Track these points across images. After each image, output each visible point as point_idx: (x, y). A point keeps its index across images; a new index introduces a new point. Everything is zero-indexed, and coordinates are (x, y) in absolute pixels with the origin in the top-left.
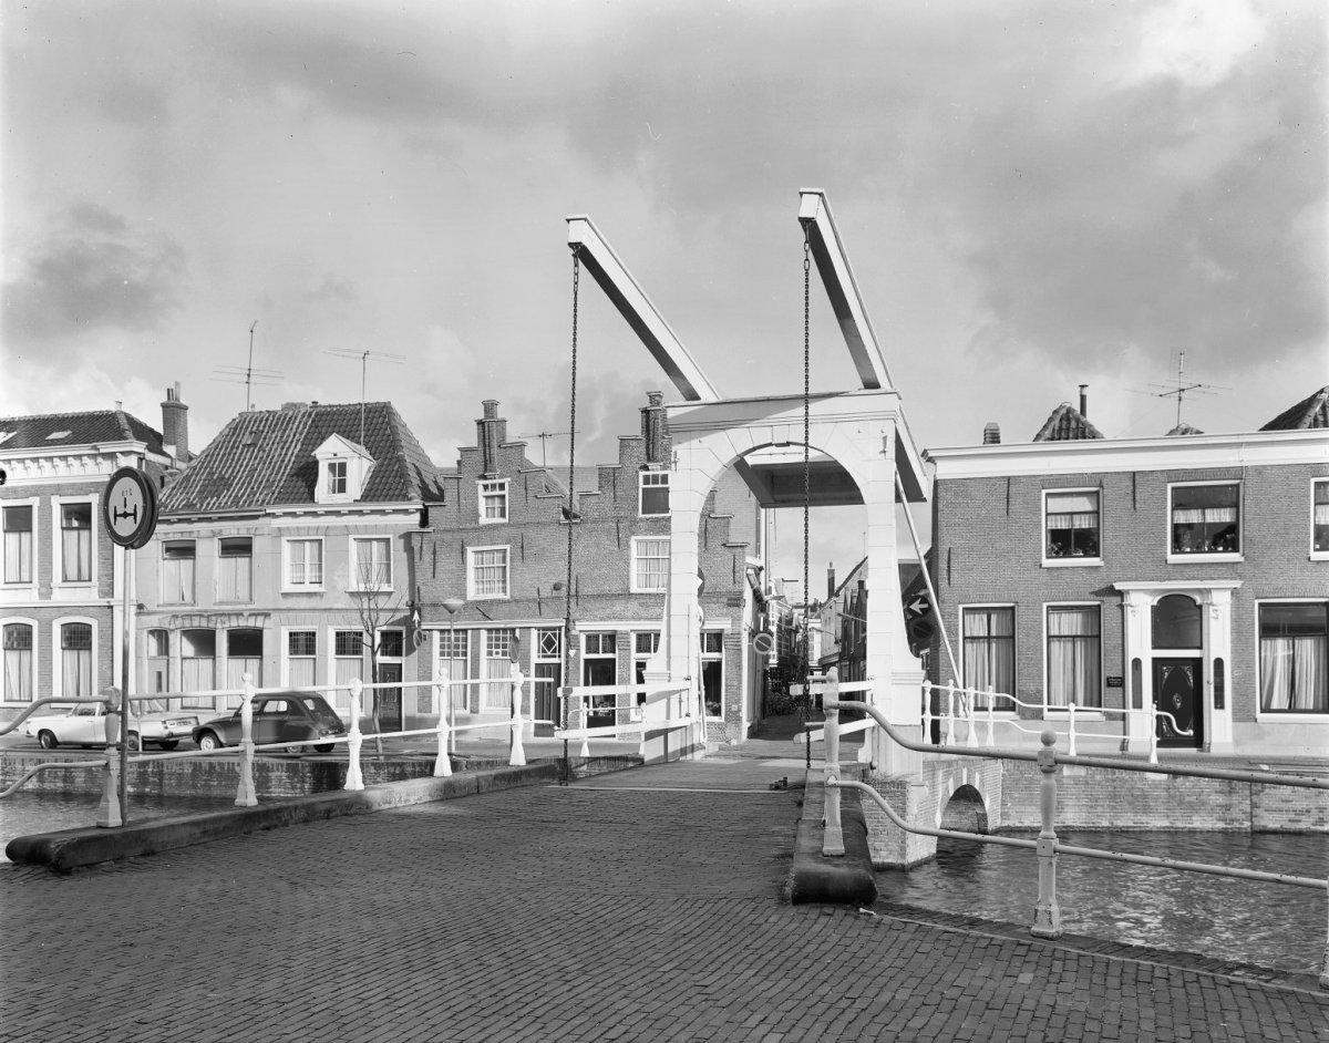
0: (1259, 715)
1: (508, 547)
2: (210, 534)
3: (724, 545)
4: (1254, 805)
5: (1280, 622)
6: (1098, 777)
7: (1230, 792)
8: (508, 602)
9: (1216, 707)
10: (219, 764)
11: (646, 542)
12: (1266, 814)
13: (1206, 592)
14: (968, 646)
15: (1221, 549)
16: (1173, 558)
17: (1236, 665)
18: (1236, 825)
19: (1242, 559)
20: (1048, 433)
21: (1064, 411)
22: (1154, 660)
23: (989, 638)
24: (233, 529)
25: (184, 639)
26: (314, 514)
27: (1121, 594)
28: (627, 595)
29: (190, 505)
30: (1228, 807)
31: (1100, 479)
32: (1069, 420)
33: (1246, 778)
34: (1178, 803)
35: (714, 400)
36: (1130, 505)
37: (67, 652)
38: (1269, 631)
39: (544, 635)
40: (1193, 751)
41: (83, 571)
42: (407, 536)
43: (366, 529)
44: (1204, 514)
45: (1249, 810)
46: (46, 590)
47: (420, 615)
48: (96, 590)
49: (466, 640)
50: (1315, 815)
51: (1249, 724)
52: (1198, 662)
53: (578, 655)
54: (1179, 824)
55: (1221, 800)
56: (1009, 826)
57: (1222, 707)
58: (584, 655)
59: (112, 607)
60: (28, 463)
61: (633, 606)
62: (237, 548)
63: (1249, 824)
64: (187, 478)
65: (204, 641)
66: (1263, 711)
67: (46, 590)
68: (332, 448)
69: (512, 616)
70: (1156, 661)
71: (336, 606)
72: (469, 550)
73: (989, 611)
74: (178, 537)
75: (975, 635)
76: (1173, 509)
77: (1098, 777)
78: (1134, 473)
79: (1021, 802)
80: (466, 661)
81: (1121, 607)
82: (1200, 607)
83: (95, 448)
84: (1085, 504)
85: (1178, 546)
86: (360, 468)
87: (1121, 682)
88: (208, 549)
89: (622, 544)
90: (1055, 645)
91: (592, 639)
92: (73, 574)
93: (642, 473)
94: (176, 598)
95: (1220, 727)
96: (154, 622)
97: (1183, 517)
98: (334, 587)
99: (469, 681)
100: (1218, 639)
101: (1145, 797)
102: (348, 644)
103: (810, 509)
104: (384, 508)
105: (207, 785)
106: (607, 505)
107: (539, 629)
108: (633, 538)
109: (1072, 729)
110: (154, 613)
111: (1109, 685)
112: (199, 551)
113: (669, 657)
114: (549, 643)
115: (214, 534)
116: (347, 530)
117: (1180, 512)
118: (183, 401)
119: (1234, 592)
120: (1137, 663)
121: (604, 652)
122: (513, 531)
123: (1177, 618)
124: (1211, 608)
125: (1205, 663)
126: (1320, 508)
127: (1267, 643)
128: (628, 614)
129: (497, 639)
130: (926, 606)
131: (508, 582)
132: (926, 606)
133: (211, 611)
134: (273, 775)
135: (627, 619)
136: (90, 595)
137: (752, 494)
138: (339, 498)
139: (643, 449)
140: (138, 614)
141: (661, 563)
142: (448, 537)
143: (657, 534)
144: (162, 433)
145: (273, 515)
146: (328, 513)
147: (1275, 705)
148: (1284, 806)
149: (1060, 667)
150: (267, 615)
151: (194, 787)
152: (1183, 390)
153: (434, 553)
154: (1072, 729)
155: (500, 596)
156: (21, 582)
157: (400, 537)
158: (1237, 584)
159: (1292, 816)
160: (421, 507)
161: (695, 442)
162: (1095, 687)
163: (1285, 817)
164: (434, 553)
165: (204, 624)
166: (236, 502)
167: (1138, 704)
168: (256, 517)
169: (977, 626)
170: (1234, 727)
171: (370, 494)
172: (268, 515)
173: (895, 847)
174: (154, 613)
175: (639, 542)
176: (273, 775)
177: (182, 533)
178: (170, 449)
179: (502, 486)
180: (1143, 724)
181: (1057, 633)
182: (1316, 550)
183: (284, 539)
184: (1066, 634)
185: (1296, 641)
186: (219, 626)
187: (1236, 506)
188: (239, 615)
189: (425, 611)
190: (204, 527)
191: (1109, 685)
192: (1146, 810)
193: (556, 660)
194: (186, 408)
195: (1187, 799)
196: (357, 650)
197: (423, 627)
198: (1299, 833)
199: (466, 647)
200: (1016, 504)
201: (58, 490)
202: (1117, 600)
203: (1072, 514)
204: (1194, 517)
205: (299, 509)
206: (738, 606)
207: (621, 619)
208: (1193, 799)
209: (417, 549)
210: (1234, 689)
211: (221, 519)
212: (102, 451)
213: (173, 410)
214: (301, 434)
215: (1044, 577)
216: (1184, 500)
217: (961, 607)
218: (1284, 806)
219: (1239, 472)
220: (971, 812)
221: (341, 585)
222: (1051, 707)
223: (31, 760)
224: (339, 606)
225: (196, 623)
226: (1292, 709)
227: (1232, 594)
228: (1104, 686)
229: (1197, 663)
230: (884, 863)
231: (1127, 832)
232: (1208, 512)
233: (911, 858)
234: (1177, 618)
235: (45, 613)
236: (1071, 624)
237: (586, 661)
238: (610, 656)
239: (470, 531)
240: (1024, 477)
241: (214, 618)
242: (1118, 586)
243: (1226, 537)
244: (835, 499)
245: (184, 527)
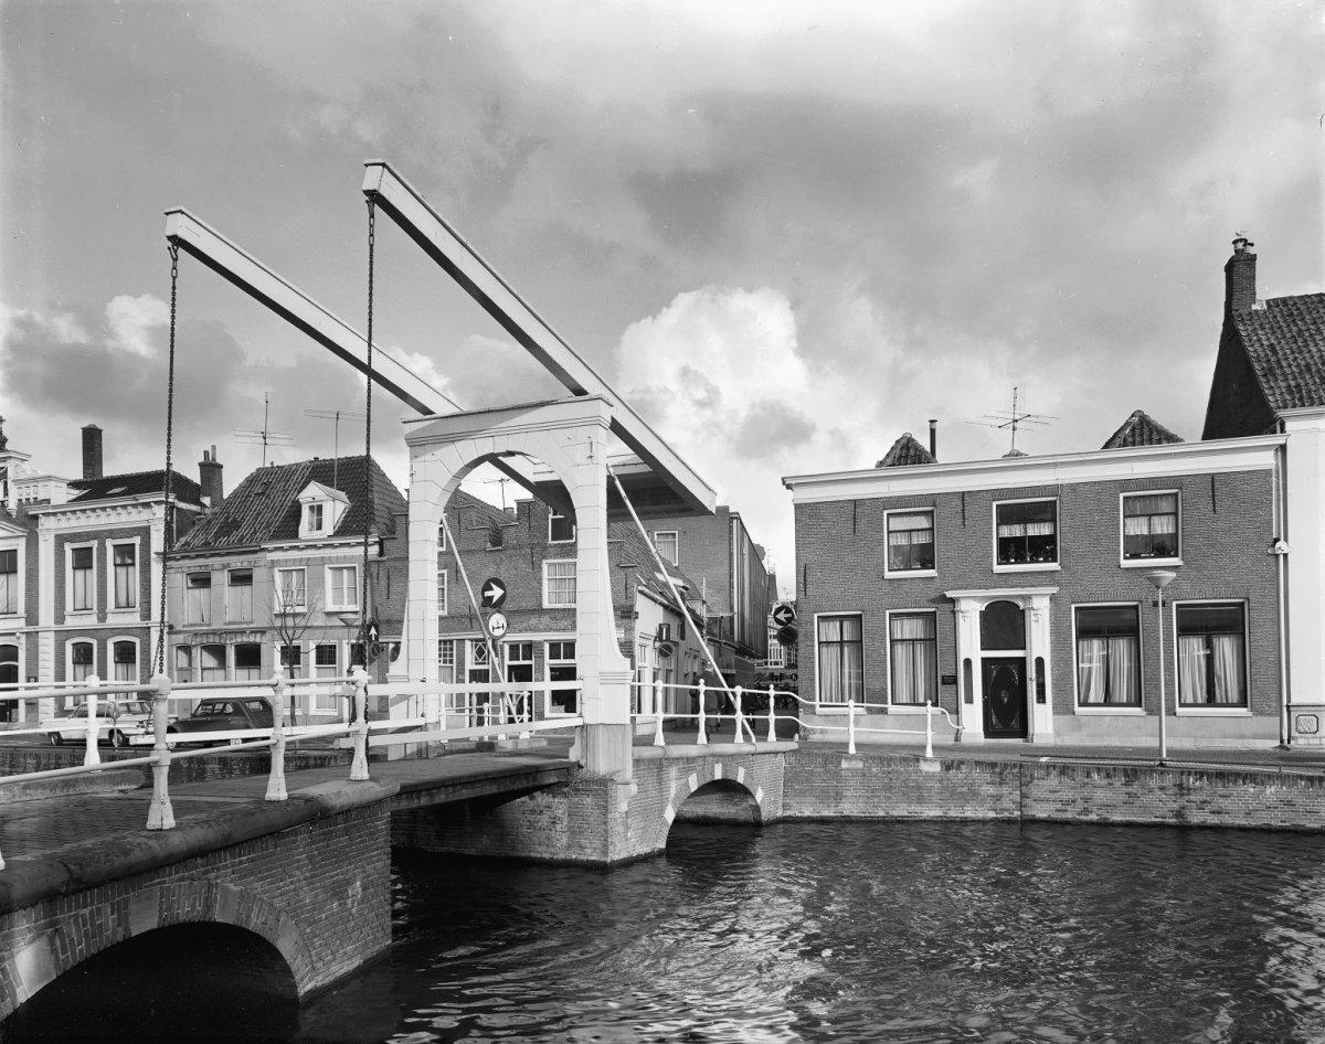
0: (1077, 709)
3: (618, 565)
4: (1024, 796)
5: (1098, 624)
6: (874, 770)
7: (1001, 784)
9: (1038, 702)
11: (555, 564)
12: (1034, 804)
13: (1027, 598)
14: (824, 650)
15: (1041, 559)
16: (998, 569)
17: (1055, 664)
18: (1006, 814)
19: (1059, 568)
20: (889, 461)
21: (904, 441)
22: (983, 659)
23: (841, 643)
24: (238, 562)
25: (205, 653)
26: (297, 548)
27: (953, 601)
28: (540, 611)
29: (207, 544)
30: (998, 798)
31: (933, 499)
32: (908, 449)
33: (1066, 763)
34: (952, 794)
35: (452, 410)
36: (960, 522)
37: (119, 665)
38: (1085, 633)
39: (476, 645)
40: (1019, 741)
41: (120, 597)
44: (1025, 529)
45: (1019, 800)
46: (102, 617)
47: (377, 630)
49: (451, 649)
50: (1080, 805)
51: (1068, 717)
52: (1023, 660)
54: (952, 814)
55: (991, 790)
56: (790, 816)
57: (1044, 702)
58: (508, 662)
59: (149, 628)
60: (69, 515)
61: (546, 619)
62: (241, 578)
63: (1019, 813)
64: (209, 522)
65: (218, 652)
66: (1080, 705)
67: (102, 617)
68: (314, 491)
70: (985, 661)
71: (315, 624)
73: (842, 618)
74: (197, 570)
75: (905, 637)
76: (998, 525)
77: (874, 770)
78: (963, 493)
79: (802, 793)
81: (954, 612)
82: (1023, 611)
83: (135, 499)
84: (923, 523)
85: (1004, 558)
86: (335, 508)
87: (953, 680)
88: (221, 579)
89: (537, 568)
90: (899, 648)
91: (514, 648)
92: (123, 601)
94: (199, 621)
95: (1043, 721)
96: (180, 639)
97: (1006, 532)
99: (637, 684)
100: (1039, 641)
101: (919, 788)
103: (164, 468)
104: (348, 541)
106: (524, 534)
107: (471, 640)
108: (544, 561)
109: (852, 725)
110: (181, 632)
111: (944, 683)
112: (213, 581)
114: (480, 652)
115: (224, 567)
117: (1005, 527)
118: (219, 461)
119: (1053, 598)
120: (968, 663)
123: (1004, 623)
124: (1032, 612)
125: (1028, 661)
126: (1128, 521)
127: (1084, 644)
128: (541, 627)
129: (445, 649)
130: (789, 615)
131: (446, 602)
132: (789, 615)
134: (208, 767)
135: (540, 631)
136: (133, 619)
137: (405, 495)
138: (317, 534)
140: (169, 633)
141: (569, 583)
144: (199, 483)
147: (1091, 700)
148: (1052, 796)
149: (906, 670)
150: (262, 632)
152: (1017, 421)
153: (388, 578)
154: (852, 725)
156: (86, 609)
158: (1055, 590)
159: (1059, 806)
160: (377, 539)
161: (428, 457)
162: (934, 686)
163: (1052, 806)
164: (388, 578)
166: (241, 540)
167: (969, 700)
168: (255, 552)
169: (832, 632)
170: (1055, 721)
171: (343, 530)
172: (263, 550)
173: (597, 844)
174: (181, 632)
175: (549, 565)
176: (208, 767)
178: (206, 501)
180: (972, 717)
181: (899, 637)
182: (1125, 558)
184: (908, 637)
185: (1110, 642)
187: (1054, 520)
188: (242, 632)
189: (382, 628)
190: (216, 561)
191: (944, 683)
192: (920, 800)
194: (221, 467)
195: (959, 790)
197: (380, 640)
198: (1065, 823)
199: (451, 655)
200: (862, 523)
201: (112, 534)
202: (948, 606)
203: (910, 531)
204: (1016, 531)
205: (285, 545)
206: (629, 617)
207: (536, 631)
208: (965, 789)
210: (1054, 685)
211: (228, 554)
212: (141, 501)
213: (211, 469)
215: (887, 588)
216: (1008, 515)
217: (816, 616)
218: (1052, 796)
219: (1055, 489)
220: (744, 804)
221: (319, 606)
222: (823, 703)
225: (212, 640)
226: (1108, 702)
227: (1051, 600)
229: (1021, 663)
230: (588, 861)
231: (908, 821)
232: (1029, 526)
233: (618, 852)
234: (1004, 623)
235: (102, 634)
236: (912, 629)
237: (510, 667)
238: (527, 662)
240: (869, 499)
242: (949, 594)
243: (1042, 548)
244: (667, 512)
245: (202, 561)
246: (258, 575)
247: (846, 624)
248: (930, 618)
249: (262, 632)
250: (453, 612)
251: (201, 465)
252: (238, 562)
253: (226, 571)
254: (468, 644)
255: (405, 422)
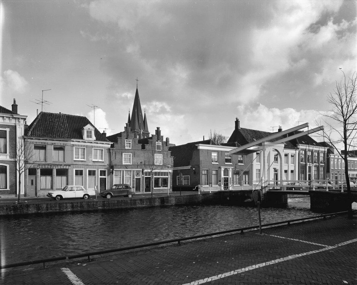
1: (131, 154)
2: (51, 144)
8: (132, 165)
10: (124, 200)
24: (59, 143)
42: (109, 149)
43: (97, 147)
48: (9, 156)
53: (144, 176)
69: (132, 168)
71: (89, 164)
72: (123, 154)
74: (41, 144)
80: (120, 177)
83: (12, 116)
88: (50, 148)
93: (156, 142)
98: (89, 160)
102: (92, 173)
104: (109, 143)
105: (121, 205)
113: (265, 177)
114: (138, 174)
115: (52, 144)
116: (92, 147)
121: (148, 176)
122: (132, 151)
127: (42, 177)
133: (52, 164)
134: (137, 202)
139: (156, 137)
142: (119, 151)
143: (159, 154)
145: (73, 141)
146: (88, 142)
150: (69, 165)
151: (118, 206)
153: (115, 154)
155: (129, 164)
157: (107, 149)
164: (115, 154)
165: (49, 167)
176: (137, 202)
177: (42, 143)
179: (130, 141)
183: (74, 147)
186: (54, 168)
188: (61, 165)
193: (139, 177)
196: (94, 174)
200: (209, 154)
209: (111, 153)
214: (65, 121)
221: (90, 159)
223: (69, 203)
224: (90, 164)
228: (218, 181)
239: (124, 150)
241: (53, 166)
246: (66, 148)
247: (205, 171)
248: (217, 171)
249: (69, 165)
250: (133, 164)
251: (12, 106)
252: (59, 143)
253: (53, 145)
254: (125, 171)
255: (37, 110)
